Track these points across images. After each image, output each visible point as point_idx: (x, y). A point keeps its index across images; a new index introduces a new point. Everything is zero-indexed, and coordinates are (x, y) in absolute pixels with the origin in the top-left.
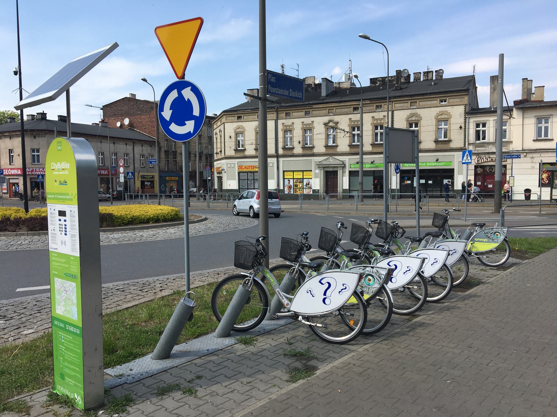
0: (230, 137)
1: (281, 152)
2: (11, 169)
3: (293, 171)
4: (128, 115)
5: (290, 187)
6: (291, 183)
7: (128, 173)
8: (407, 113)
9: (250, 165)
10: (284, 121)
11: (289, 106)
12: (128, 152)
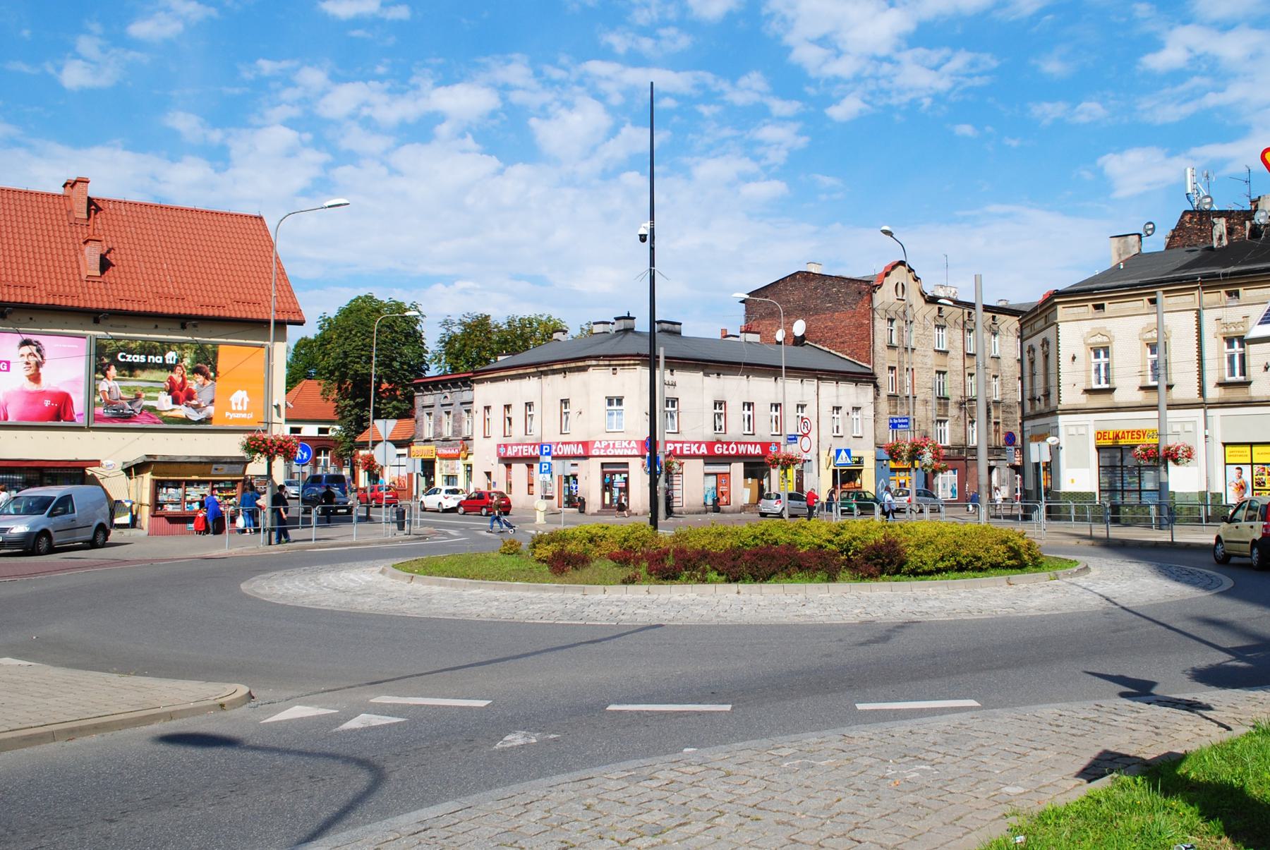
0: (1074, 358)
1: (1213, 393)
2: (564, 443)
3: (1251, 444)
4: (803, 312)
5: (1242, 487)
6: (1247, 477)
7: (838, 452)
8: (1087, 326)
9: (1136, 428)
10: (1218, 313)
11: (1233, 274)
12: (805, 400)
